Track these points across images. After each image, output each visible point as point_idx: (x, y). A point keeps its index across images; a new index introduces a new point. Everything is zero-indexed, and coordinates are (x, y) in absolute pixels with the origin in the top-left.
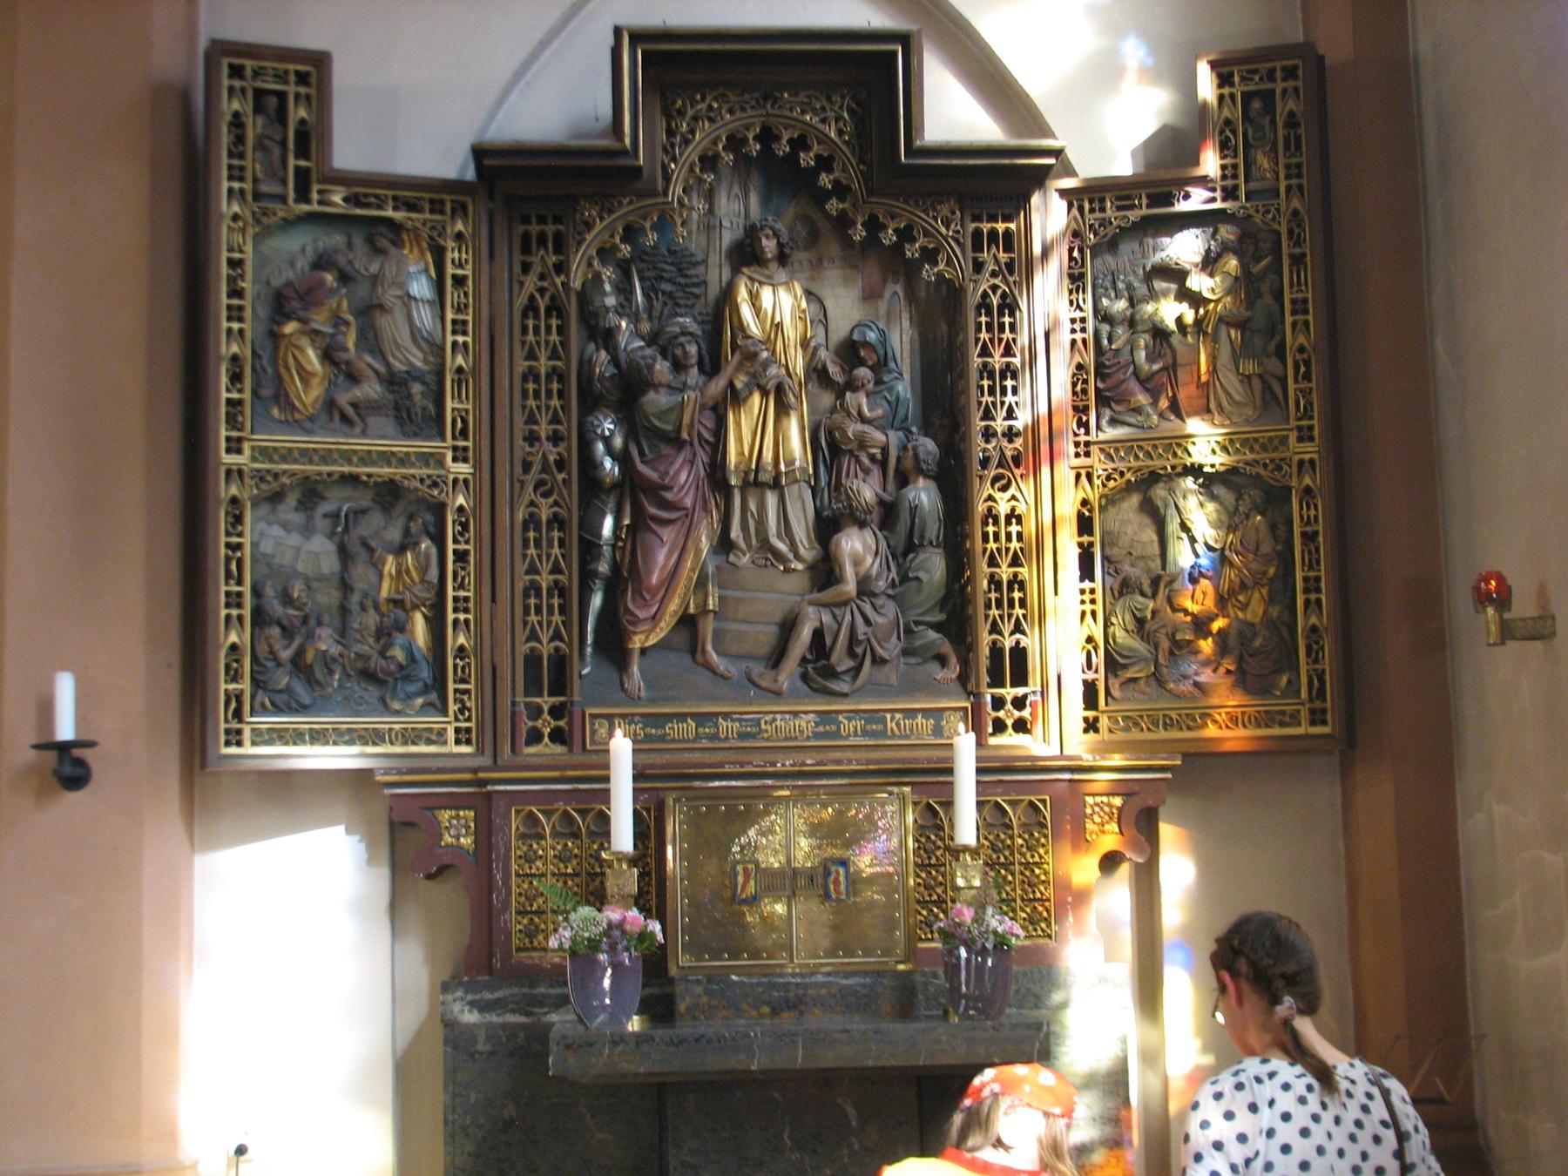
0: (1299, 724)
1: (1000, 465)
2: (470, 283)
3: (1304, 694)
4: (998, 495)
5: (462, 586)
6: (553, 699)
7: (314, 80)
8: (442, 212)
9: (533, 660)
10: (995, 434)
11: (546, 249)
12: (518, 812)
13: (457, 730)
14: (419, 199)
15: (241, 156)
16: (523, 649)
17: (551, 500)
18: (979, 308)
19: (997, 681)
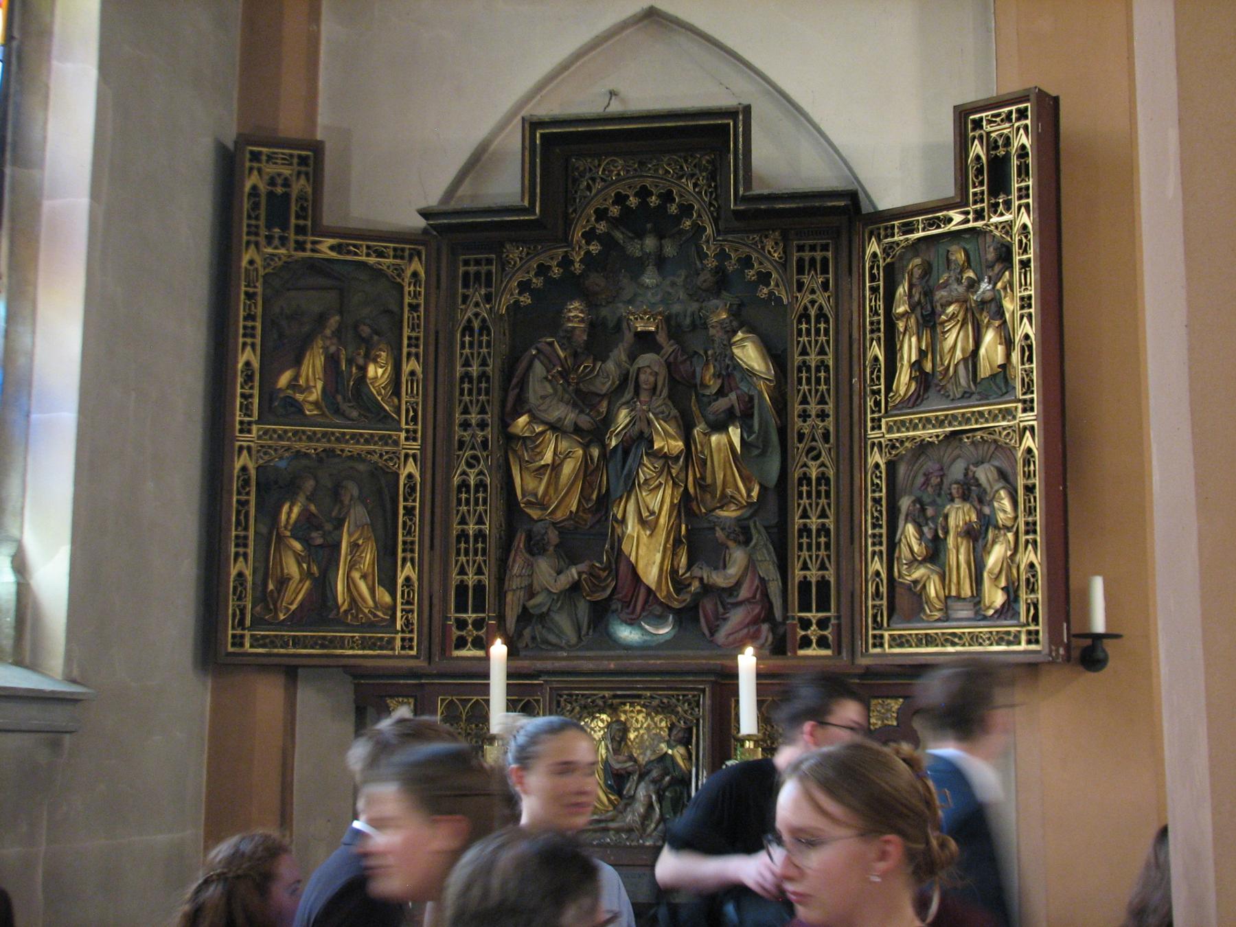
0: (1019, 643)
1: (473, 448)
2: (422, 309)
3: (1023, 619)
4: (811, 463)
5: (409, 533)
6: (820, 615)
7: (311, 162)
8: (402, 258)
9: (462, 589)
10: (470, 425)
11: (816, 271)
12: (443, 700)
13: (403, 639)
14: (386, 247)
15: (257, 218)
16: (455, 578)
17: (818, 462)
18: (801, 317)
19: (805, 607)
